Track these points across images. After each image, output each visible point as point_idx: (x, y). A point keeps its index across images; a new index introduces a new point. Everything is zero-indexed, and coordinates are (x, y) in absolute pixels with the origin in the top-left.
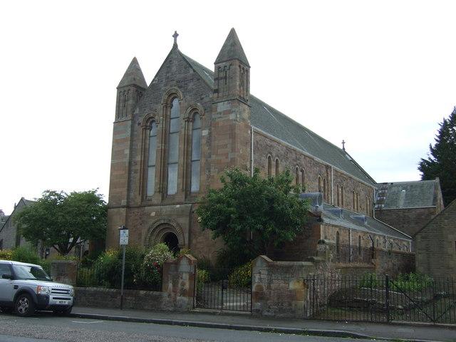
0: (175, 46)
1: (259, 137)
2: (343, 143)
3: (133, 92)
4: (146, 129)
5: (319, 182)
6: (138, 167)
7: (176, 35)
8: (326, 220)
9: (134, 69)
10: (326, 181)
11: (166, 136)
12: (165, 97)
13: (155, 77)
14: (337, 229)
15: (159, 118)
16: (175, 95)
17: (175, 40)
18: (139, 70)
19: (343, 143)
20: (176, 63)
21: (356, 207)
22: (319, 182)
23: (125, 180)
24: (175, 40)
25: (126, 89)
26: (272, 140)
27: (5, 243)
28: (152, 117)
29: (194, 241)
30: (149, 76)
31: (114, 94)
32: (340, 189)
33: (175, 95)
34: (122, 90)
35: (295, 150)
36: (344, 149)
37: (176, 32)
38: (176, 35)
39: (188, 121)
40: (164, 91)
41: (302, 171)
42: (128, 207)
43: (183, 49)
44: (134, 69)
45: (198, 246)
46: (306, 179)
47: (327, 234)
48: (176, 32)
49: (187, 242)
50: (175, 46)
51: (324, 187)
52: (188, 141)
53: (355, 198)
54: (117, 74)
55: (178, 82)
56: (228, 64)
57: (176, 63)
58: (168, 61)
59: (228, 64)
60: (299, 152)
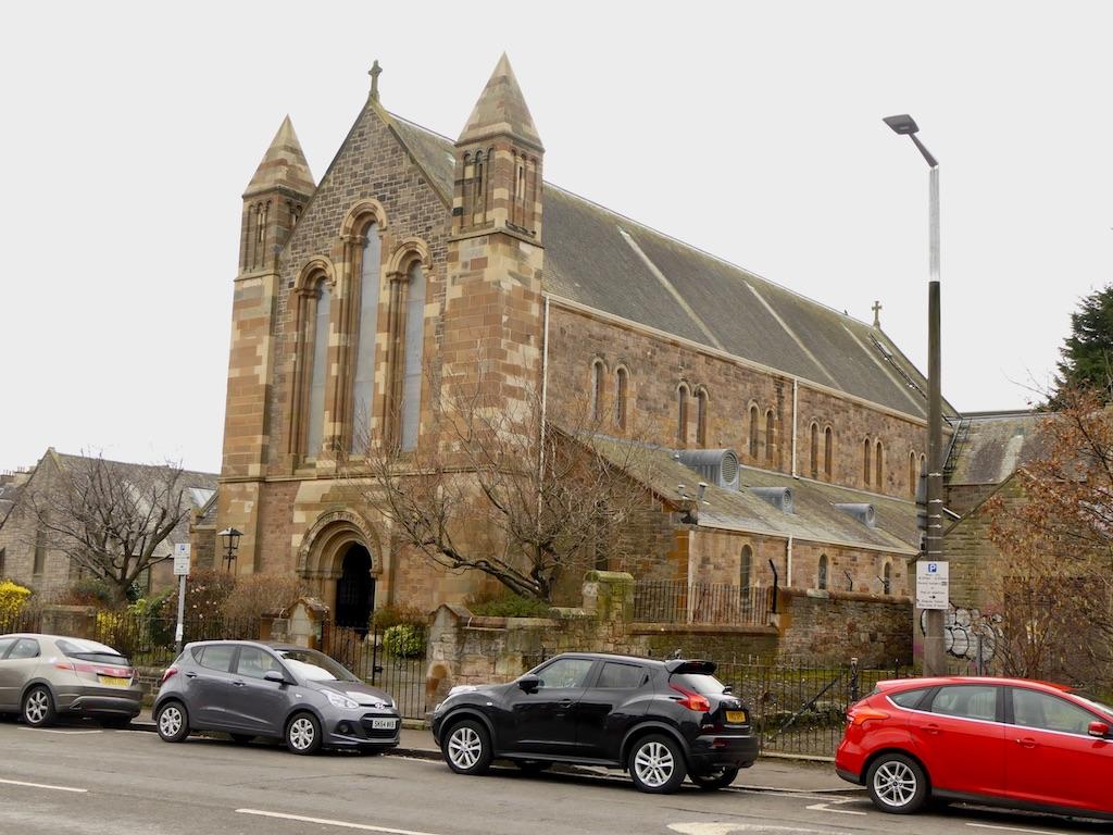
0: (374, 95)
1: (566, 319)
2: (877, 308)
3: (281, 208)
4: (306, 297)
5: (754, 421)
6: (288, 387)
7: (375, 72)
8: (704, 520)
9: (285, 153)
10: (776, 418)
11: (349, 317)
12: (349, 222)
13: (328, 172)
14: (746, 541)
15: (337, 271)
16: (371, 218)
17: (374, 83)
18: (296, 151)
19: (877, 308)
20: (377, 137)
21: (873, 480)
22: (754, 421)
23: (257, 416)
24: (374, 83)
25: (264, 198)
26: (605, 323)
27: (10, 559)
28: (321, 270)
29: (403, 564)
30: (317, 170)
31: (238, 209)
32: (822, 436)
33: (371, 218)
34: (256, 202)
35: (675, 344)
36: (877, 324)
37: (376, 63)
38: (375, 72)
39: (398, 281)
40: (347, 206)
41: (700, 395)
42: (262, 480)
43: (390, 103)
44: (285, 153)
45: (413, 575)
46: (710, 416)
47: (710, 554)
48: (376, 63)
49: (386, 566)
50: (374, 95)
51: (769, 434)
52: (396, 325)
53: (873, 457)
54: (240, 171)
55: (378, 186)
56: (484, 147)
57: (377, 137)
58: (358, 131)
59: (484, 147)
60: (690, 349)
